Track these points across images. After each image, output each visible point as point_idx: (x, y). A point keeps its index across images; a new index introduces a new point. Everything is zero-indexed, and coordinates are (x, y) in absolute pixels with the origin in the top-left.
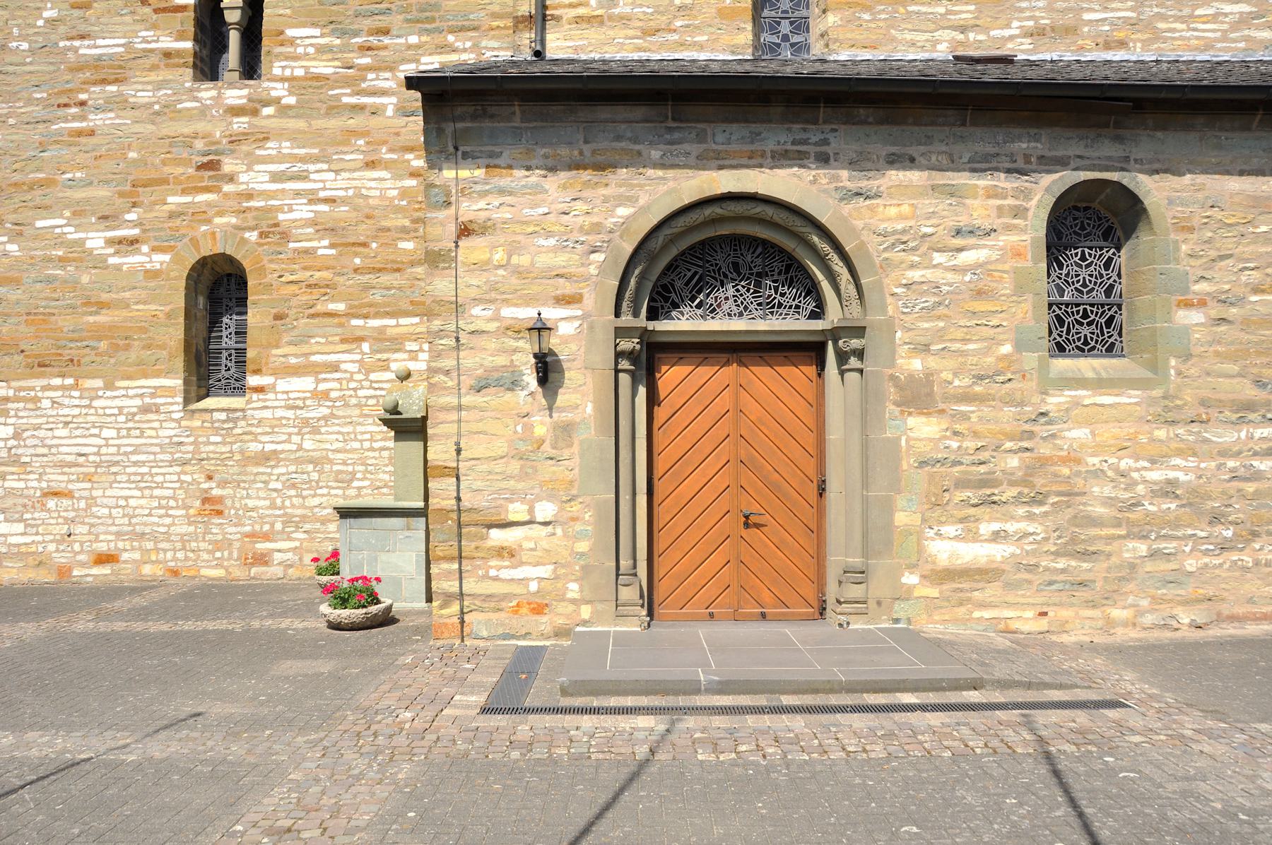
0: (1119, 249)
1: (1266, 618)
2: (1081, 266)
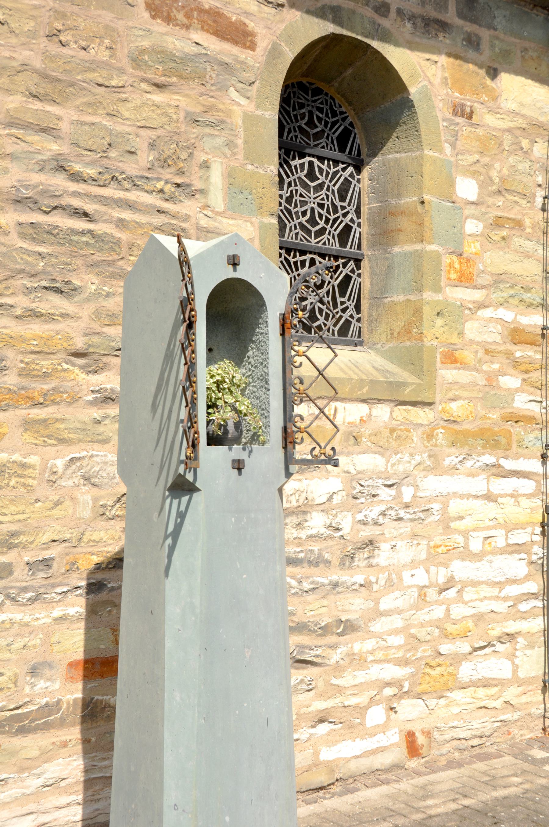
0: (358, 169)
1: (5, 805)
2: (307, 134)
